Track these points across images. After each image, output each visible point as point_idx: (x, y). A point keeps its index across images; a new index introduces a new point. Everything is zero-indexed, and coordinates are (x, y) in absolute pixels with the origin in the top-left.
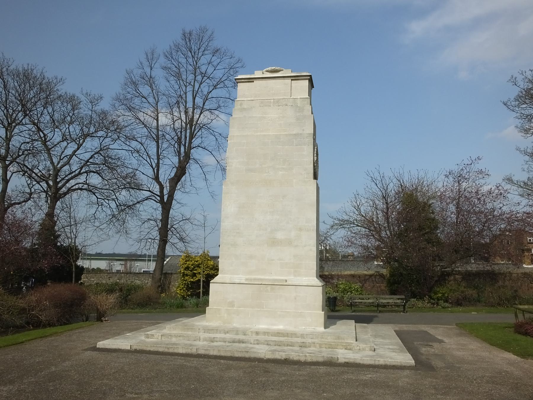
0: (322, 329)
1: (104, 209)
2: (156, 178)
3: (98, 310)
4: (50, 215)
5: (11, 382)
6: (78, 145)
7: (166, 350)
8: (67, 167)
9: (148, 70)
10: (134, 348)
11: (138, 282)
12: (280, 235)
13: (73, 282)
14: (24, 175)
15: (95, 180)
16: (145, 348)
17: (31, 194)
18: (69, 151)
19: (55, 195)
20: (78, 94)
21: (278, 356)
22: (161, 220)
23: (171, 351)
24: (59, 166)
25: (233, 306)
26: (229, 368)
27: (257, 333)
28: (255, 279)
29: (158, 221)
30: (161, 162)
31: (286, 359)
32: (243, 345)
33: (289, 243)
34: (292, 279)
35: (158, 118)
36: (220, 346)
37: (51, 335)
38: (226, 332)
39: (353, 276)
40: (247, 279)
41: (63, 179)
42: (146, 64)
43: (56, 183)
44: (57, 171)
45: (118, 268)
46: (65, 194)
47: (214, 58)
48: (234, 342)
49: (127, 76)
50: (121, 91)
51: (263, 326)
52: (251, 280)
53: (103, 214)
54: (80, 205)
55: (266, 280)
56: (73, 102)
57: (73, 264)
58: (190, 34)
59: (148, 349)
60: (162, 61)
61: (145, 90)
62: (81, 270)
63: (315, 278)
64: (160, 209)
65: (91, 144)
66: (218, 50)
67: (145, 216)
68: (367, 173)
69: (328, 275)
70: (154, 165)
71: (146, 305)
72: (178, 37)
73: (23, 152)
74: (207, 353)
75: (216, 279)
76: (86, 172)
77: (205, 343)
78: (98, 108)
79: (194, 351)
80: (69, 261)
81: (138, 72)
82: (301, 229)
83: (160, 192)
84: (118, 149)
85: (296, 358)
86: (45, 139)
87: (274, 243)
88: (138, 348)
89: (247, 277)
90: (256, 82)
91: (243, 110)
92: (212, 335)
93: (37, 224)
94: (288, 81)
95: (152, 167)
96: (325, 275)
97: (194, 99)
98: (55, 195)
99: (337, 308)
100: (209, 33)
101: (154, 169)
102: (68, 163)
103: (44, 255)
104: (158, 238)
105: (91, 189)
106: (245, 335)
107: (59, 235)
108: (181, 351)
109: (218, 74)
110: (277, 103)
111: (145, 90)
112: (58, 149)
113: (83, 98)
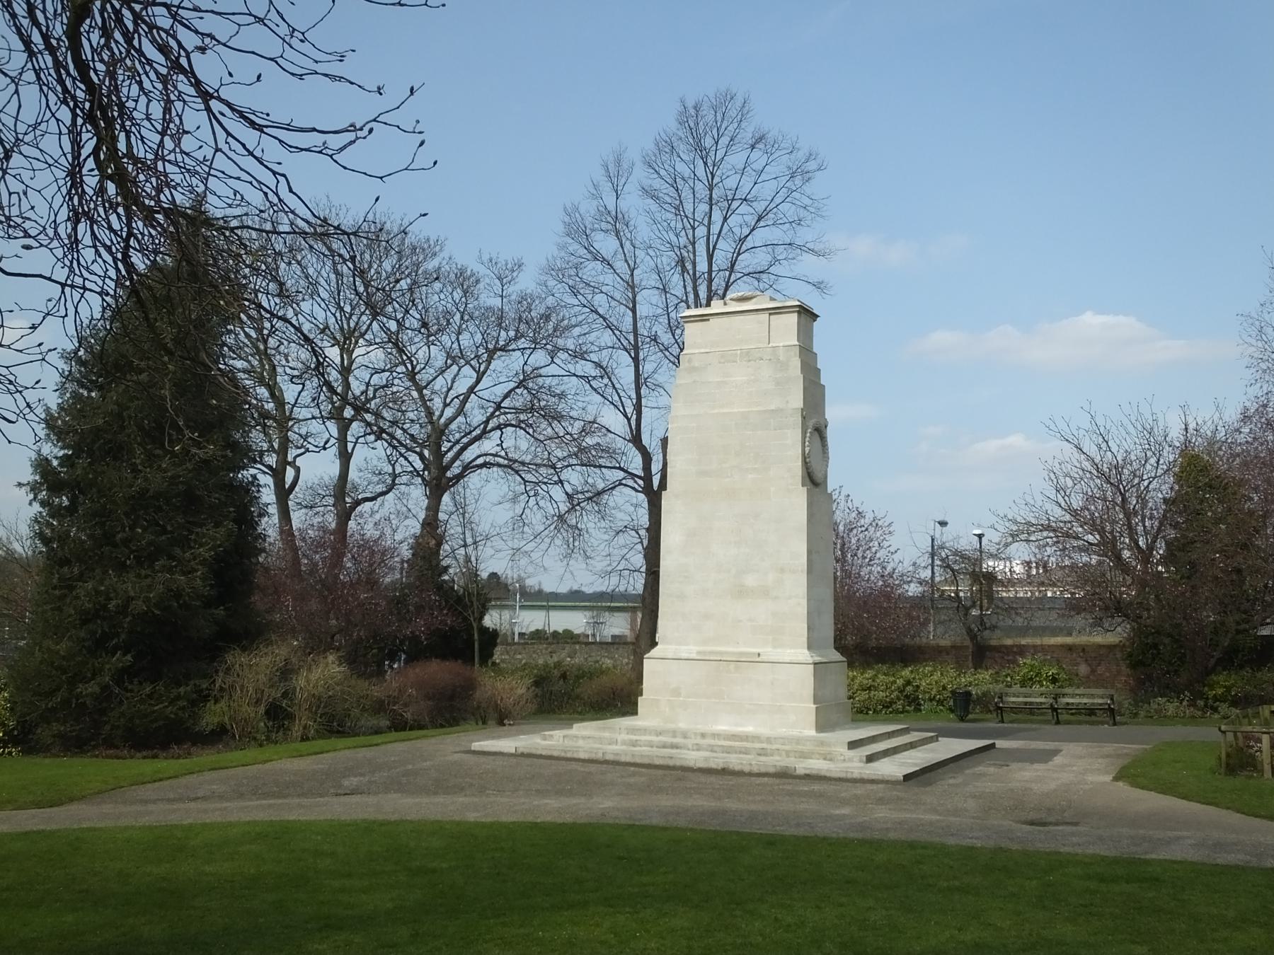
0: (813, 733)
1: (542, 503)
2: (636, 439)
3: (497, 705)
4: (431, 524)
5: (362, 775)
6: (478, 372)
7: (563, 754)
8: (461, 419)
9: (610, 202)
10: (520, 751)
11: (608, 662)
12: (750, 581)
13: (477, 660)
14: (379, 438)
15: (517, 443)
16: (534, 751)
17: (394, 476)
18: (462, 387)
19: (439, 482)
20: (473, 266)
21: (712, 765)
22: (647, 530)
23: (569, 755)
24: (442, 420)
25: (679, 695)
26: (634, 774)
27: (703, 735)
28: (712, 653)
29: (643, 532)
30: (644, 401)
31: (723, 769)
32: (674, 751)
33: (765, 592)
34: (769, 652)
35: (634, 306)
36: (644, 752)
37: (417, 738)
38: (659, 733)
39: (1070, 648)
40: (699, 653)
41: (458, 442)
42: (606, 188)
43: (439, 455)
44: (439, 432)
45: (617, 631)
46: (459, 477)
47: (756, 154)
48: (664, 747)
49: (567, 219)
50: (556, 253)
51: (722, 727)
52: (704, 653)
53: (539, 515)
54: (487, 499)
55: (726, 653)
56: (464, 282)
57: (475, 625)
58: (697, 108)
59: (539, 752)
60: (641, 175)
61: (606, 244)
62: (491, 638)
63: (806, 651)
64: (646, 505)
65: (506, 368)
66: (761, 139)
67: (621, 518)
68: (1049, 423)
69: (1012, 646)
70: (629, 410)
71: (608, 705)
72: (669, 122)
73: (376, 391)
74: (617, 758)
75: (655, 652)
76: (499, 427)
77: (624, 747)
78: (514, 290)
79: (600, 756)
80: (465, 619)
81: (588, 208)
82: (782, 570)
83: (644, 469)
84: (556, 373)
85: (737, 768)
86: (414, 368)
87: (741, 592)
88: (526, 751)
89: (701, 648)
90: (713, 321)
91: (692, 370)
92: (634, 738)
93: (405, 546)
94: (765, 316)
95: (625, 415)
96: (1006, 647)
97: (710, 257)
98: (439, 482)
99: (970, 716)
100: (738, 102)
101: (629, 420)
102: (460, 411)
103: (420, 608)
104: (643, 569)
105: (512, 466)
106: (685, 737)
107: (446, 569)
108: (582, 756)
109: (766, 190)
110: (748, 356)
111: (606, 244)
112: (440, 384)
113: (481, 270)
